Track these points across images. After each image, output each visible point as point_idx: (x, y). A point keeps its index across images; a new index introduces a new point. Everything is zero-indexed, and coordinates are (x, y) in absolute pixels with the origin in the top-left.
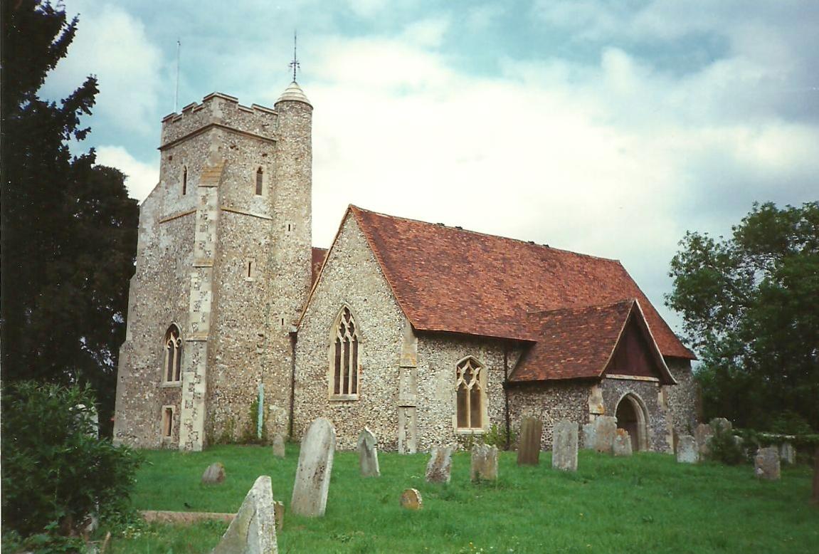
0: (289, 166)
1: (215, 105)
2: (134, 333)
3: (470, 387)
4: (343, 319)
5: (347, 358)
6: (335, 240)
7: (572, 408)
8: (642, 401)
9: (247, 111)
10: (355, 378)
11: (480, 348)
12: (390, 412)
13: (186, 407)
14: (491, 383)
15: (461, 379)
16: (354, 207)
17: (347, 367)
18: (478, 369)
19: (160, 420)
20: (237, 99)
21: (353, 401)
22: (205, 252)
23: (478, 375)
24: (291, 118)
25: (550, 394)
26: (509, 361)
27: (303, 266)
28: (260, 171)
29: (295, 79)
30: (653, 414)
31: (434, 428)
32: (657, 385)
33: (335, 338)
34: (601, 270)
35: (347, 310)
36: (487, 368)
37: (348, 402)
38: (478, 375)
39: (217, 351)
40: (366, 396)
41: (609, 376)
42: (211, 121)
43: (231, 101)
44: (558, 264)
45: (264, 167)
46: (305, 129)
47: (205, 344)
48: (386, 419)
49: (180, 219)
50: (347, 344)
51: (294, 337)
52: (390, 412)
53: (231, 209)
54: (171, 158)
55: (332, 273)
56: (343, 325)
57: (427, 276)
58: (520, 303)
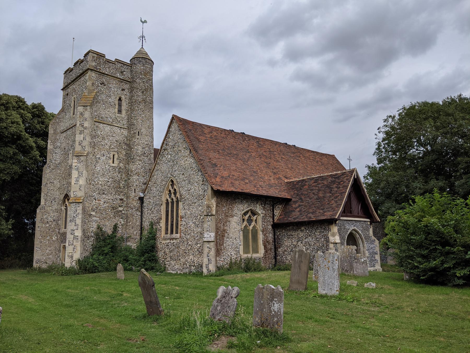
0: (139, 96)
1: (89, 58)
2: (46, 200)
3: (251, 227)
4: (170, 187)
5: (172, 211)
6: (165, 138)
7: (318, 239)
8: (361, 233)
9: (111, 63)
10: (177, 224)
11: (257, 203)
12: (199, 245)
13: (69, 245)
14: (340, 224)
15: (245, 223)
16: (175, 116)
17: (172, 217)
18: (256, 216)
19: (60, 252)
20: (105, 55)
21: (176, 239)
22: (82, 146)
23: (256, 220)
24: (139, 67)
25: (302, 231)
26: (275, 211)
27: (147, 157)
28: (120, 99)
29: (142, 46)
30: (367, 241)
31: (228, 255)
32: (369, 223)
33: (165, 199)
34: (325, 160)
35: (172, 181)
36: (262, 215)
37: (173, 239)
38: (256, 220)
39: (92, 209)
40: (184, 236)
41: (341, 218)
42: (88, 66)
43: (101, 56)
44: (301, 155)
45: (123, 97)
46: (149, 73)
47: (81, 204)
48: (196, 250)
49: (71, 130)
50: (172, 203)
51: (141, 199)
52: (199, 245)
53: (101, 121)
54: (67, 94)
55: (163, 159)
56: (170, 191)
57: (223, 159)
58: (281, 176)
